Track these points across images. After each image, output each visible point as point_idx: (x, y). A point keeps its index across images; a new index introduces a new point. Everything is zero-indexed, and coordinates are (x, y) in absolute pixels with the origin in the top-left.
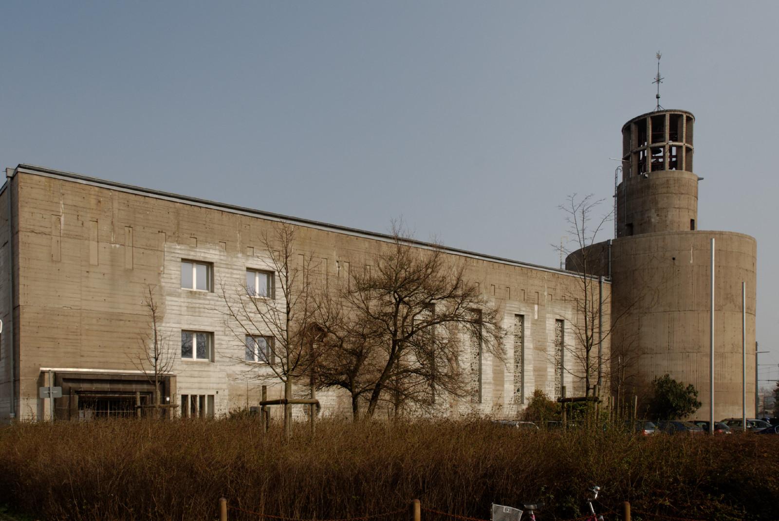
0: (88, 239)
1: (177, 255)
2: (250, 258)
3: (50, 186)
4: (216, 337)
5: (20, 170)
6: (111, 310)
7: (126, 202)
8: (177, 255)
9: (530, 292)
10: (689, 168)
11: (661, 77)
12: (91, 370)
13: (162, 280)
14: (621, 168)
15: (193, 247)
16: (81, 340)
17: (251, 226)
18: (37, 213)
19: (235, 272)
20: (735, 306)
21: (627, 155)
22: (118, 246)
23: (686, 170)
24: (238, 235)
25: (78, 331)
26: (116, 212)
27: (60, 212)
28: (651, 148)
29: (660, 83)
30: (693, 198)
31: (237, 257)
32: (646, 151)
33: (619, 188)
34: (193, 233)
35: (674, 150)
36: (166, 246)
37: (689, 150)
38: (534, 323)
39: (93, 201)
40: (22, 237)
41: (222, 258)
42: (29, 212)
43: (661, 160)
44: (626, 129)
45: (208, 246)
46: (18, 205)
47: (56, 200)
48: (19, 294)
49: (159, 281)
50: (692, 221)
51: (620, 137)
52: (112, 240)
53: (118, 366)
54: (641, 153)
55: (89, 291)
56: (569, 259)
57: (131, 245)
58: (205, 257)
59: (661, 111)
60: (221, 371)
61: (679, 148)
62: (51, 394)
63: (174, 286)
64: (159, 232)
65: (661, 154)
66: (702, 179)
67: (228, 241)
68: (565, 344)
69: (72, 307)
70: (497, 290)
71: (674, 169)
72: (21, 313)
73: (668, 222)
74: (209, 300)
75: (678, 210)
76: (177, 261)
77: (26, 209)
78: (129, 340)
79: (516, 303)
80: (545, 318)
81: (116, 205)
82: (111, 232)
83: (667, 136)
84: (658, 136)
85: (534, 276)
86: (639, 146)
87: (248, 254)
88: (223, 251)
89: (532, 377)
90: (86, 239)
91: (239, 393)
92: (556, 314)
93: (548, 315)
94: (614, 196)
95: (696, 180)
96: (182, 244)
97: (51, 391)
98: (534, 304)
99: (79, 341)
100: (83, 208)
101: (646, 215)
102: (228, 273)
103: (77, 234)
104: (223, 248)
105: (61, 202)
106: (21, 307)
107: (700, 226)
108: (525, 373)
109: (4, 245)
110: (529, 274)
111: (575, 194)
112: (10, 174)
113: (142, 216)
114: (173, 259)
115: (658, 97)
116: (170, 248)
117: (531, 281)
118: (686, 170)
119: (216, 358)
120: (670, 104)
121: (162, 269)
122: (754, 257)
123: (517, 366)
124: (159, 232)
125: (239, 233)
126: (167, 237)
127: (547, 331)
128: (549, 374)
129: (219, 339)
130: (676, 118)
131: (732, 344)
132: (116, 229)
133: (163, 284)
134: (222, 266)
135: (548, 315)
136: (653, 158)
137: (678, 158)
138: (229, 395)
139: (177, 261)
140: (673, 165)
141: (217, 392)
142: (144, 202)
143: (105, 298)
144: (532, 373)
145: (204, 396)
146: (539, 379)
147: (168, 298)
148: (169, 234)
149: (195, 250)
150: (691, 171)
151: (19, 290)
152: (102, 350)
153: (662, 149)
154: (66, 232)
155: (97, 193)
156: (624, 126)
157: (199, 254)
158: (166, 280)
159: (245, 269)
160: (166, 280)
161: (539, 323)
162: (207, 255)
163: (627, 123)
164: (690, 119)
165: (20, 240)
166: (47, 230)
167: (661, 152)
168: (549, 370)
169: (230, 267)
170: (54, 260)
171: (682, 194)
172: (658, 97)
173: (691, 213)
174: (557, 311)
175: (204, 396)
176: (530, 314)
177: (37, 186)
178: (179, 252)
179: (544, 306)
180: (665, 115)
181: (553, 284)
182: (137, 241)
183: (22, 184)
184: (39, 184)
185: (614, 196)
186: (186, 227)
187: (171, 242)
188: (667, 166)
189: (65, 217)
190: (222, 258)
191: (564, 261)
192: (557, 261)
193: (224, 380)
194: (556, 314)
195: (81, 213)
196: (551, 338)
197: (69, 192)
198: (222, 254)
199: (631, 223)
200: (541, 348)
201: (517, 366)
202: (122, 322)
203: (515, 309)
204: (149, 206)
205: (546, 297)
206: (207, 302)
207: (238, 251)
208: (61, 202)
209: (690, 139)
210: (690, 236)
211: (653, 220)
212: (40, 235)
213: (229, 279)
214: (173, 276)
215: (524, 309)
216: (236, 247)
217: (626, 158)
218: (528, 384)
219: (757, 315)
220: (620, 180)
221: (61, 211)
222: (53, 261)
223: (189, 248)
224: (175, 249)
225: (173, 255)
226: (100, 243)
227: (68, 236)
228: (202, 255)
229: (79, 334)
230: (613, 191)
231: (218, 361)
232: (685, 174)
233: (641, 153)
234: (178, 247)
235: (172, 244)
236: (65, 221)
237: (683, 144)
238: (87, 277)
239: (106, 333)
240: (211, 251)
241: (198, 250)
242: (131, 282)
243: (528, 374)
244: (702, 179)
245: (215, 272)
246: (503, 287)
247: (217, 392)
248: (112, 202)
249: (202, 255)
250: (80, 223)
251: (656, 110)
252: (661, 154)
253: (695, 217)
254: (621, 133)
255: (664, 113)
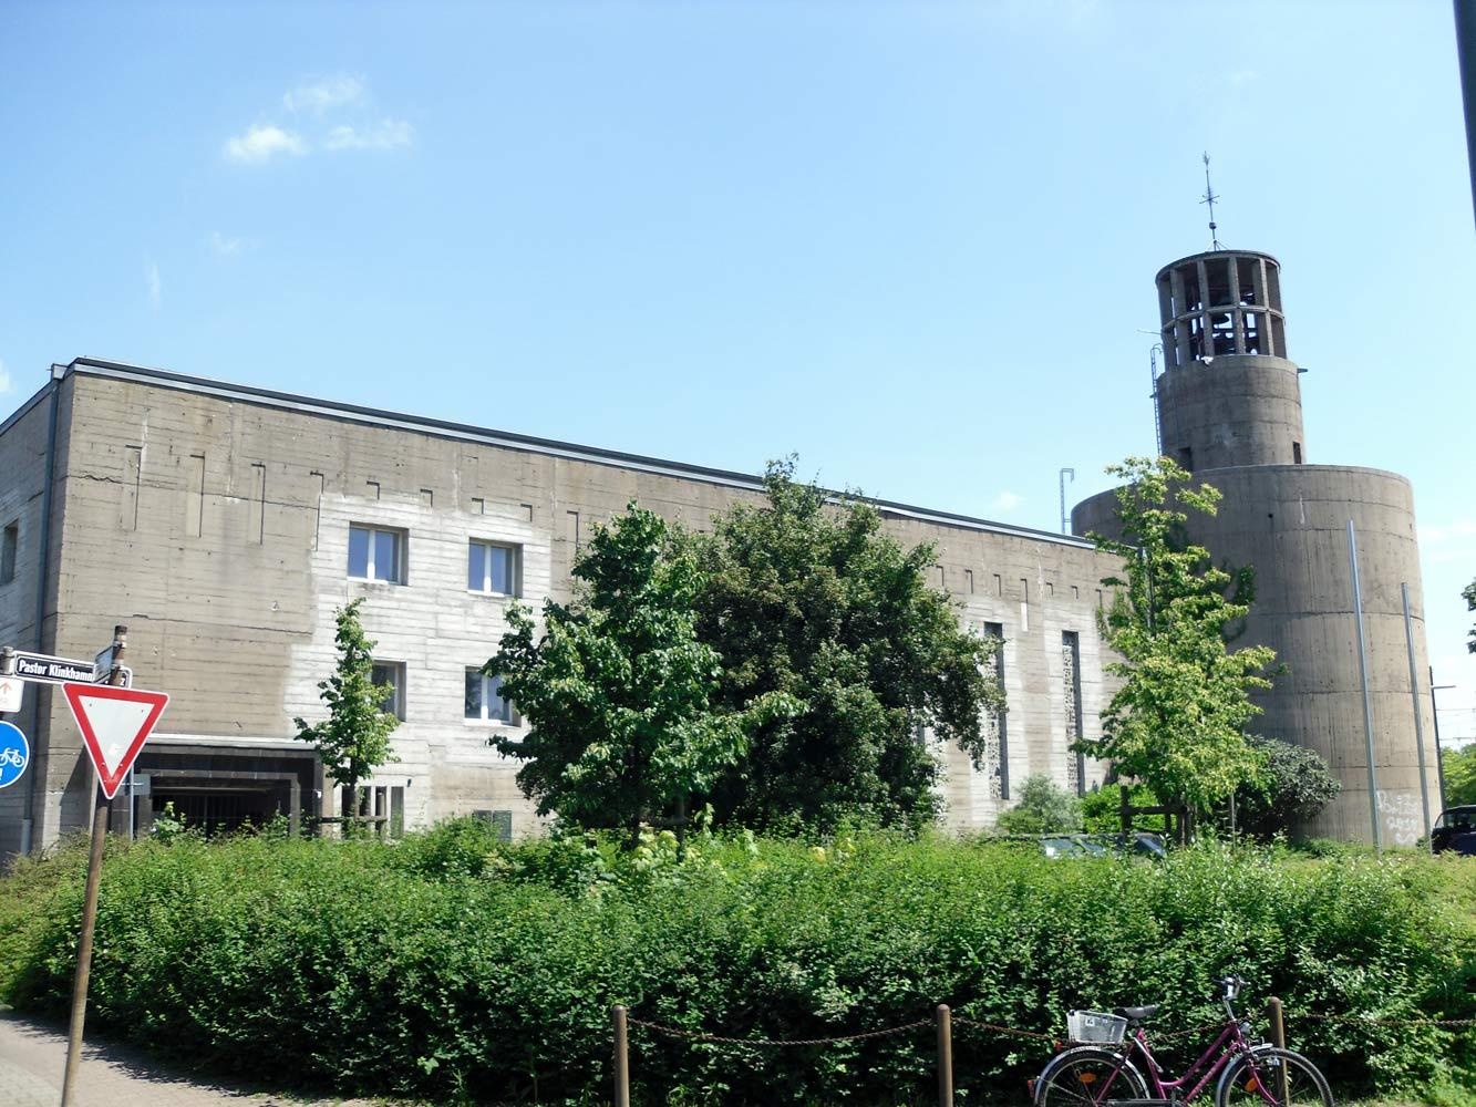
0: (185, 489)
1: (342, 516)
2: (477, 519)
3: (127, 395)
4: (409, 672)
5: (78, 367)
6: (218, 621)
7: (257, 420)
8: (342, 516)
9: (1011, 579)
10: (1281, 351)
11: (1214, 195)
12: (205, 737)
13: (314, 563)
14: (1160, 347)
15: (372, 500)
16: (161, 677)
17: (480, 459)
18: (100, 443)
19: (448, 545)
20: (1388, 603)
21: (1168, 324)
22: (237, 500)
23: (1276, 355)
24: (456, 476)
25: (159, 660)
26: (238, 438)
27: (140, 441)
28: (1210, 314)
29: (1213, 204)
30: (1293, 404)
31: (453, 519)
32: (1201, 319)
33: (1159, 382)
34: (375, 473)
35: (1251, 319)
36: (327, 499)
37: (1278, 322)
38: (1023, 638)
39: (199, 420)
40: (71, 486)
41: (425, 519)
42: (88, 442)
43: (1229, 335)
44: (1164, 278)
45: (400, 497)
46: (69, 429)
47: (135, 419)
48: (57, 591)
49: (308, 566)
50: (1296, 446)
51: (1154, 292)
52: (228, 490)
53: (240, 728)
54: (1194, 322)
55: (181, 586)
56: (1079, 513)
57: (261, 498)
58: (395, 519)
59: (1220, 252)
60: (418, 740)
61: (1259, 316)
62: (132, 789)
63: (334, 573)
64: (312, 473)
65: (1228, 325)
66: (1306, 371)
67: (436, 487)
68: (562, 607)
69: (150, 616)
70: (947, 576)
71: (1254, 352)
72: (59, 628)
73: (1254, 448)
74: (399, 600)
75: (1268, 425)
76: (341, 527)
77: (82, 437)
78: (247, 679)
79: (986, 600)
80: (1041, 627)
81: (238, 425)
82: (226, 474)
83: (1236, 294)
84: (1220, 295)
85: (1018, 546)
86: (1189, 309)
87: (474, 512)
88: (427, 508)
89: (1025, 747)
90: (182, 490)
91: (451, 783)
92: (1063, 620)
93: (1047, 624)
94: (1151, 397)
95: (1295, 371)
96: (353, 494)
97: (132, 783)
98: (1020, 601)
99: (158, 680)
100: (182, 432)
101: (1214, 434)
102: (434, 548)
103: (166, 479)
104: (426, 502)
105: (145, 423)
106: (59, 616)
107: (1310, 458)
108: (1009, 738)
109: (31, 499)
110: (1008, 545)
111: (1110, 470)
112: (59, 374)
113: (283, 445)
114: (334, 522)
115: (1213, 227)
116: (330, 502)
117: (1011, 559)
118: (1276, 354)
119: (408, 715)
120: (1234, 239)
121: (313, 542)
122: (1410, 513)
123: (993, 724)
124: (312, 473)
125: (457, 473)
126: (326, 482)
127: (1047, 655)
128: (1055, 738)
129: (415, 677)
130: (1248, 262)
131: (1389, 676)
132: (236, 469)
133: (315, 571)
134: (425, 534)
135: (1047, 624)
136: (1215, 331)
137: (1261, 330)
138: (433, 788)
139: (341, 527)
140: (1253, 343)
141: (409, 782)
142: (287, 419)
143: (209, 598)
144: (1022, 739)
145: (385, 788)
146: (1036, 750)
147: (323, 597)
148: (328, 476)
149: (376, 505)
150: (1284, 356)
151: (58, 584)
152: (199, 697)
153: (1229, 315)
154: (149, 477)
155: (206, 405)
156: (1159, 274)
157: (382, 513)
158: (321, 564)
159: (467, 540)
160: (321, 564)
161: (1032, 637)
162: (396, 515)
163: (1165, 268)
164: (1272, 267)
165: (67, 493)
166: (114, 474)
167: (1226, 320)
168: (1055, 730)
169: (437, 536)
170: (125, 529)
171: (1274, 397)
172: (1213, 227)
173: (1293, 432)
174: (1064, 615)
175: (385, 788)
176: (1014, 621)
177: (105, 396)
178: (346, 509)
179: (1039, 605)
180: (1228, 260)
181: (1052, 564)
182: (271, 491)
183: (80, 392)
184: (109, 391)
185: (1151, 397)
186: (360, 464)
187: (333, 491)
188: (1242, 345)
189: (149, 449)
190: (425, 519)
191: (1068, 516)
192: (1053, 518)
193: (422, 758)
194: (1063, 620)
195: (175, 442)
196: (1057, 668)
197: (159, 405)
198: (425, 512)
199: (1186, 446)
200: (1036, 687)
201: (993, 724)
202: (237, 644)
203: (985, 613)
204: (296, 426)
205: (1042, 587)
206: (394, 605)
207: (454, 507)
208: (145, 423)
209: (1275, 300)
210: (1295, 474)
211: (1226, 443)
212: (102, 483)
213: (437, 561)
214: (333, 556)
215: (1000, 612)
216: (450, 498)
217: (1167, 332)
218: (1017, 761)
219: (1426, 619)
220: (1161, 369)
221: (143, 438)
222: (121, 530)
223: (364, 502)
224: (339, 504)
225: (335, 515)
226: (205, 496)
227: (152, 483)
228: (389, 514)
229: (158, 666)
230: (1150, 389)
231: (413, 720)
232: (1275, 363)
233: (1194, 322)
234: (344, 500)
235: (334, 495)
236: (147, 455)
237: (1266, 307)
238: (180, 559)
239: (206, 664)
240: (406, 508)
241: (380, 505)
242: (256, 567)
243: (1016, 739)
244: (1306, 371)
245: (410, 546)
246: (960, 570)
247: (409, 782)
248: (232, 422)
249: (389, 514)
250: (174, 458)
251: (1213, 250)
252: (1228, 325)
253: (1301, 437)
254: (1155, 286)
255: (1227, 256)
